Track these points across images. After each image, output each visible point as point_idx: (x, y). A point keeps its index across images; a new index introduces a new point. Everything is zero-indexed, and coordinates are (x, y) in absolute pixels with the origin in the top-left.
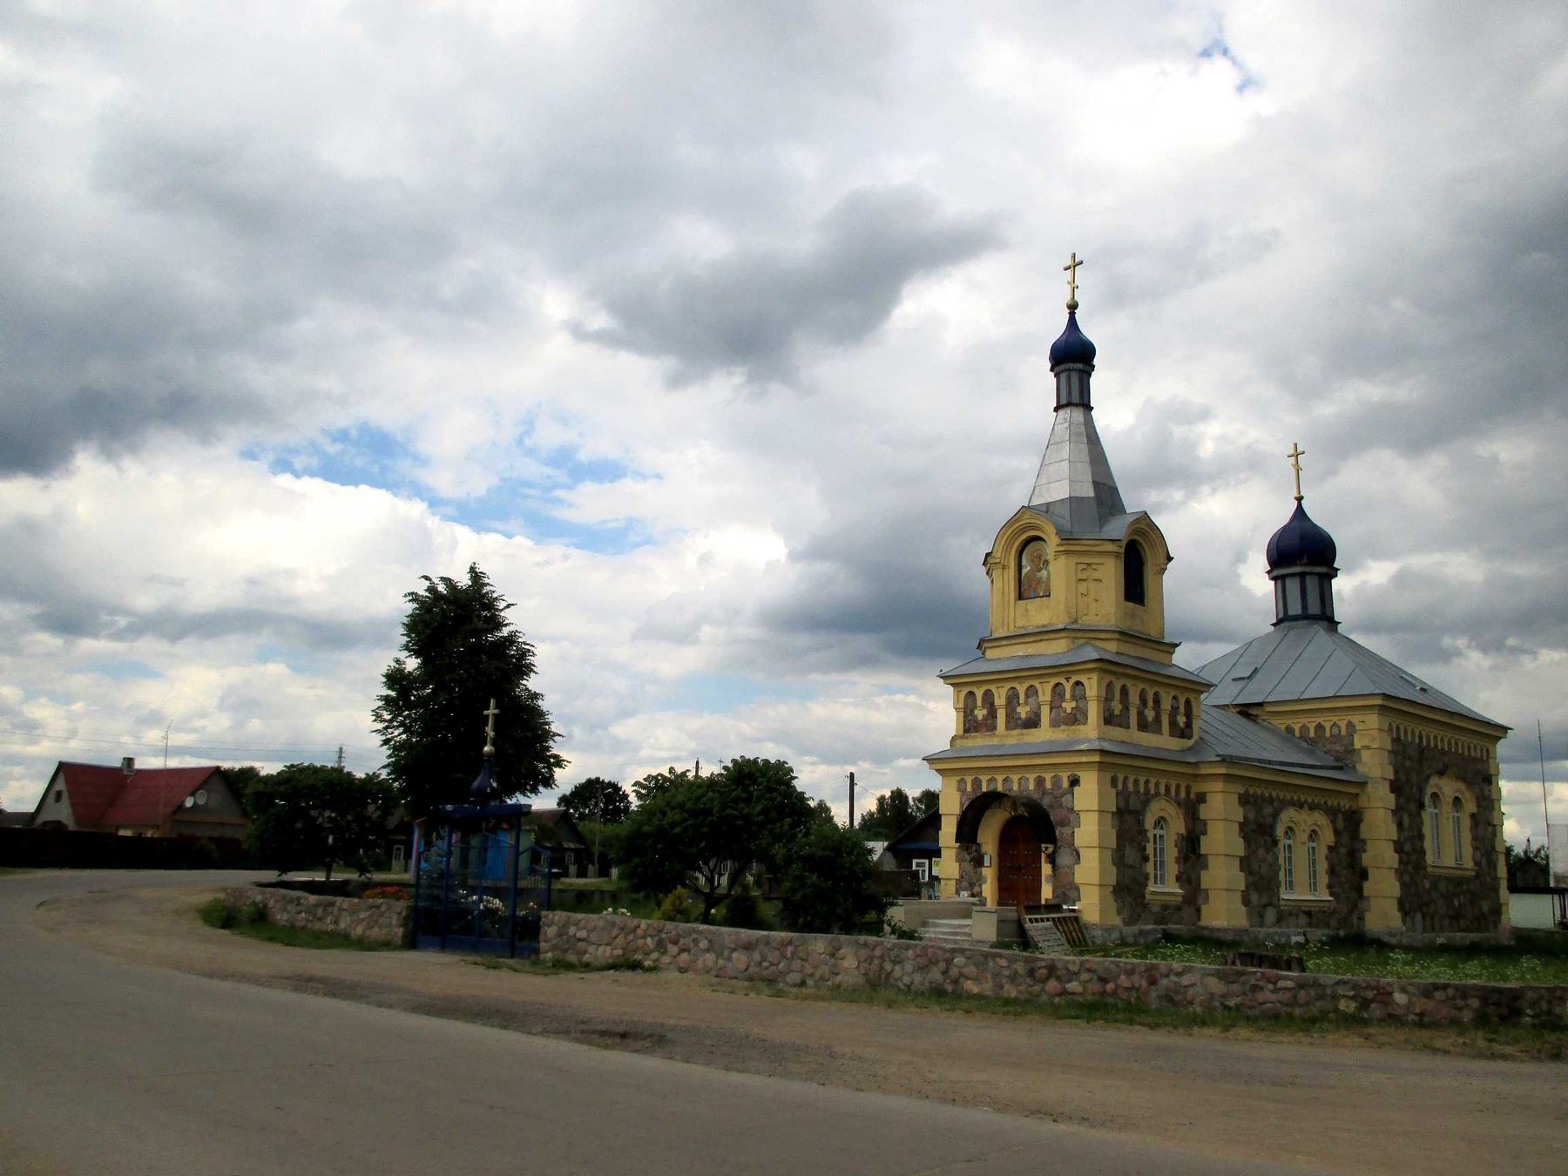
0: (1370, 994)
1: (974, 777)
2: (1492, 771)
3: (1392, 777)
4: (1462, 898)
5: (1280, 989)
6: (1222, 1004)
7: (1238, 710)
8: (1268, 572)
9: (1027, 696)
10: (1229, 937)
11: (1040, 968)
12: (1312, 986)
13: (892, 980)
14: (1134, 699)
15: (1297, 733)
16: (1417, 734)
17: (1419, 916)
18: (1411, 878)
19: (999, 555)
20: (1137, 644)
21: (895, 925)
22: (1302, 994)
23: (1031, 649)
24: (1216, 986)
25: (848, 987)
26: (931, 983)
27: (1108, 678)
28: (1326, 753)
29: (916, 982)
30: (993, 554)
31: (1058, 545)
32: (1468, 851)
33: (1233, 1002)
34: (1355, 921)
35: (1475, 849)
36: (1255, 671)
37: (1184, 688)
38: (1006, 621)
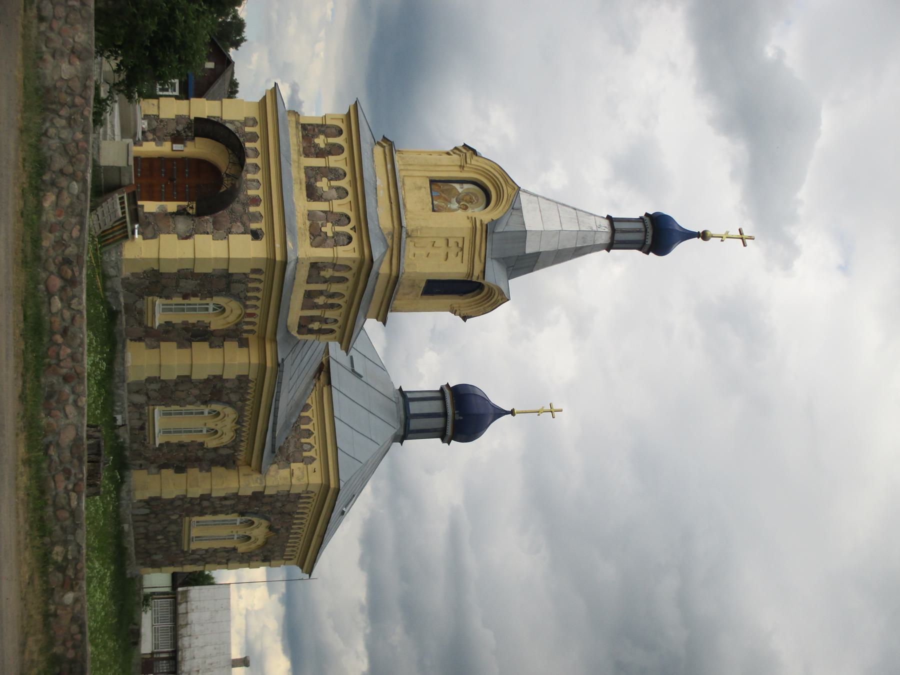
0: (70, 573)
1: (259, 135)
2: (273, 562)
3: (266, 493)
4: (164, 541)
5: (69, 495)
6: (51, 443)
7: (324, 363)
8: (448, 385)
9: (338, 188)
10: (117, 368)
11: (72, 270)
12: (74, 521)
13: (51, 116)
14: (335, 288)
15: (304, 414)
16: (305, 511)
17: (147, 511)
18: (179, 506)
19: (473, 162)
20: (385, 294)
21: (107, 104)
22: (66, 514)
23: (383, 194)
24: (67, 437)
25: (41, 68)
26: (51, 157)
27: (355, 267)
28: (287, 438)
29: (51, 142)
30: (475, 157)
31: (481, 221)
32: (204, 545)
33: (53, 454)
34: (138, 462)
35: (207, 551)
36: (359, 376)
37: (345, 330)
38: (409, 168)
